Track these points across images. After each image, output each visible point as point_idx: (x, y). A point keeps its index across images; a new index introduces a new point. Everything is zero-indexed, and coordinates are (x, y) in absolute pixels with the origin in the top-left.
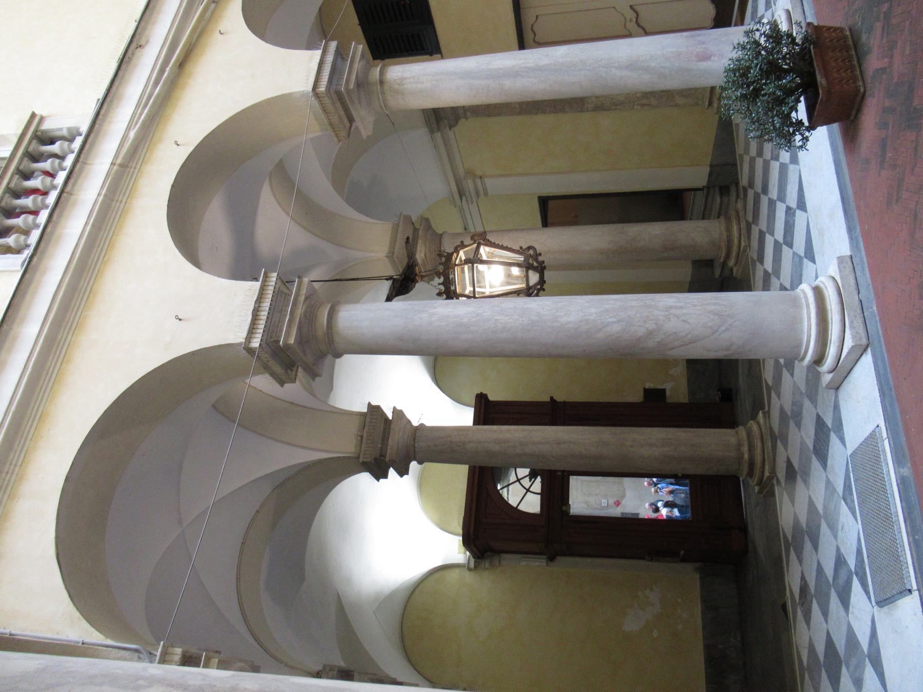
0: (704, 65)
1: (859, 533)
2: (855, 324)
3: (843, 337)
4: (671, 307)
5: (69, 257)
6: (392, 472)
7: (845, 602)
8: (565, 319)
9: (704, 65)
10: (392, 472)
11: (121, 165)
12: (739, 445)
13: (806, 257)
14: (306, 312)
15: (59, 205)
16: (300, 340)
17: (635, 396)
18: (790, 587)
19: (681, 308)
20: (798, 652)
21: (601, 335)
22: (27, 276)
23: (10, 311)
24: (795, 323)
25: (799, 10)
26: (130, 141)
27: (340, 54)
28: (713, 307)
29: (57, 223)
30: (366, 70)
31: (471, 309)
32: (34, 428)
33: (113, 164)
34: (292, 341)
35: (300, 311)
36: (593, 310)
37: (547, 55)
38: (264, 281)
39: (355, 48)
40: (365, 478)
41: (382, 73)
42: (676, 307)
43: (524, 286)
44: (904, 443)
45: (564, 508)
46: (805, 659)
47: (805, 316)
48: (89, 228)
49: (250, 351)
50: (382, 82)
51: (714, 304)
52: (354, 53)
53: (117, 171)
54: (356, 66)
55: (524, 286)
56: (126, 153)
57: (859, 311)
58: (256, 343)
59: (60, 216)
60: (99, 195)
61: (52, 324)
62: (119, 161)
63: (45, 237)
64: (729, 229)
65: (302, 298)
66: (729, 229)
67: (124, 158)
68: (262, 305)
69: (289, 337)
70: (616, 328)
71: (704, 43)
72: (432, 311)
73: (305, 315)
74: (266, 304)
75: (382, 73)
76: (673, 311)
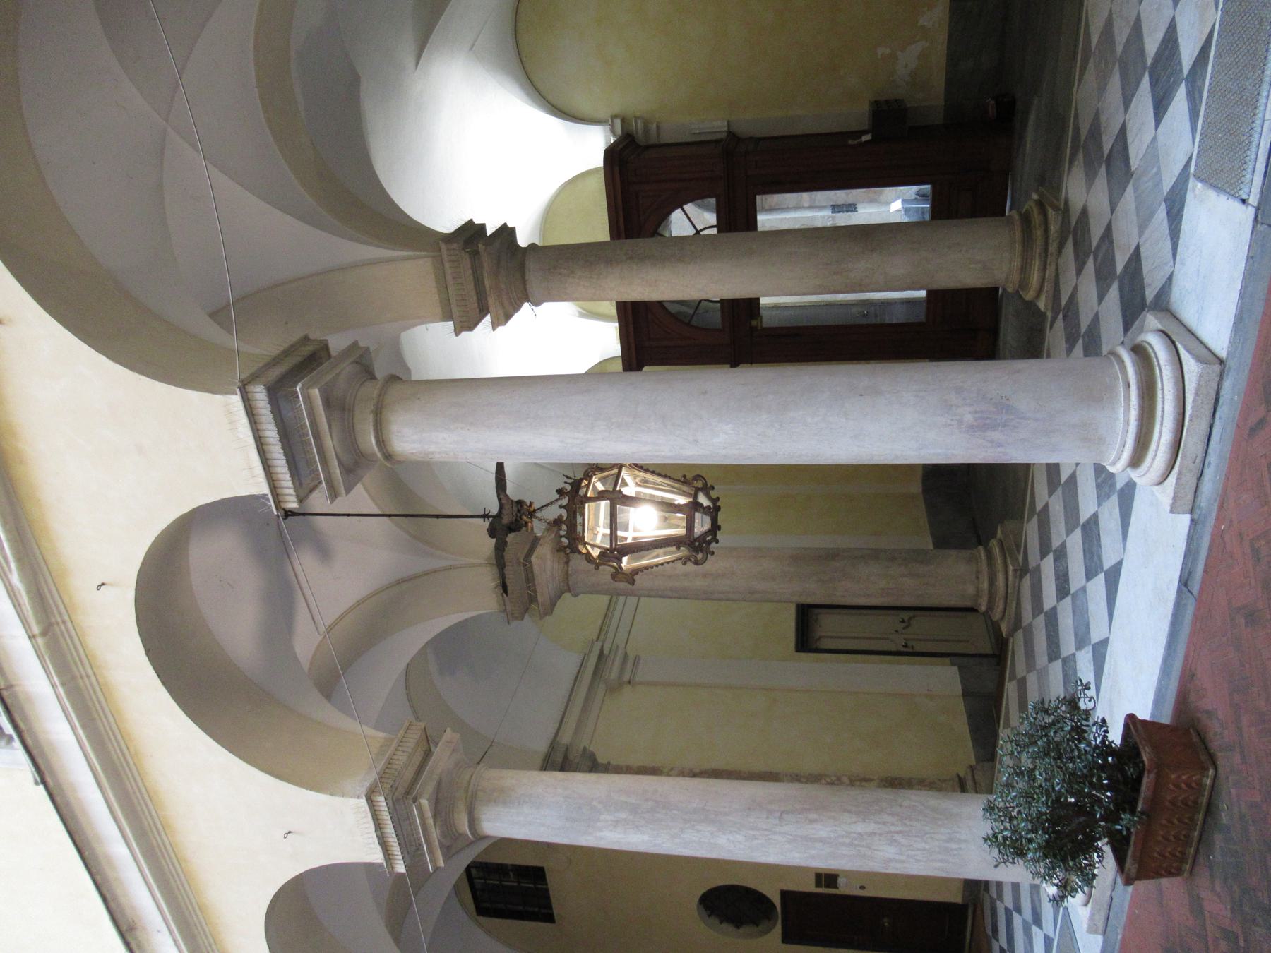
1: (1211, 33)
2: (1097, 917)
4: (890, 860)
5: (90, 773)
7: (1161, 106)
11: (44, 633)
12: (978, 595)
13: (1106, 574)
15: (12, 709)
17: (850, 113)
18: (1076, 110)
19: (903, 862)
20: (1087, 25)
22: (58, 799)
23: (77, 838)
25: (1204, 426)
26: (24, 593)
28: (940, 864)
29: (30, 729)
32: (79, 647)
33: (31, 637)
35: (435, 834)
37: (696, 441)
39: (308, 399)
42: (896, 861)
43: (681, 531)
45: (754, 323)
46: (1095, 39)
48: (80, 731)
51: (941, 861)
52: (314, 424)
53: (48, 646)
54: (329, 443)
55: (681, 531)
56: (34, 608)
57: (1106, 907)
59: (26, 719)
60: (54, 686)
61: (108, 778)
62: (36, 630)
63: (35, 752)
64: (1024, 269)
65: (430, 821)
66: (1024, 269)
67: (39, 622)
71: (1000, 445)
72: (598, 834)
73: (444, 835)
74: (390, 830)
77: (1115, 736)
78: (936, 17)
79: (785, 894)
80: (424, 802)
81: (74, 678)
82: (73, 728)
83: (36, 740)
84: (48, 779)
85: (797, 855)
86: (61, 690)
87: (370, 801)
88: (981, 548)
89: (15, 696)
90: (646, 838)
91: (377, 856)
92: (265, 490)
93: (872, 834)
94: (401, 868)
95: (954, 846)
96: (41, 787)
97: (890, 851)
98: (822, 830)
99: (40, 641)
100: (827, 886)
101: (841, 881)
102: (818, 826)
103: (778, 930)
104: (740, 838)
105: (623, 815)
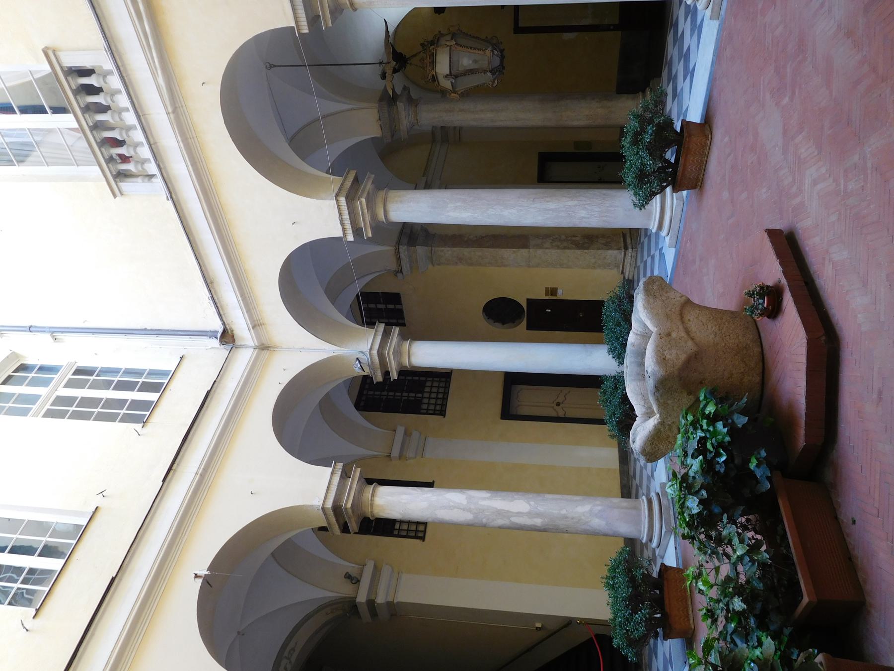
4: (583, 218)
11: (174, 112)
29: (165, 167)
31: (469, 214)
33: (168, 114)
35: (368, 218)
36: (540, 218)
62: (170, 110)
65: (366, 211)
77: (678, 127)
78: (658, 663)
79: (530, 301)
80: (363, 200)
81: (187, 139)
82: (187, 166)
83: (168, 175)
84: (173, 196)
85: (540, 218)
86: (181, 144)
87: (337, 200)
88: (616, 21)
89: (157, 147)
90: (469, 214)
91: (339, 234)
92: (293, 24)
93: (576, 205)
94: (350, 238)
95: (612, 209)
96: (170, 202)
97: (583, 213)
98: (552, 205)
99: (172, 116)
100: (552, 295)
101: (560, 291)
102: (550, 203)
103: (525, 322)
104: (514, 211)
105: (459, 204)
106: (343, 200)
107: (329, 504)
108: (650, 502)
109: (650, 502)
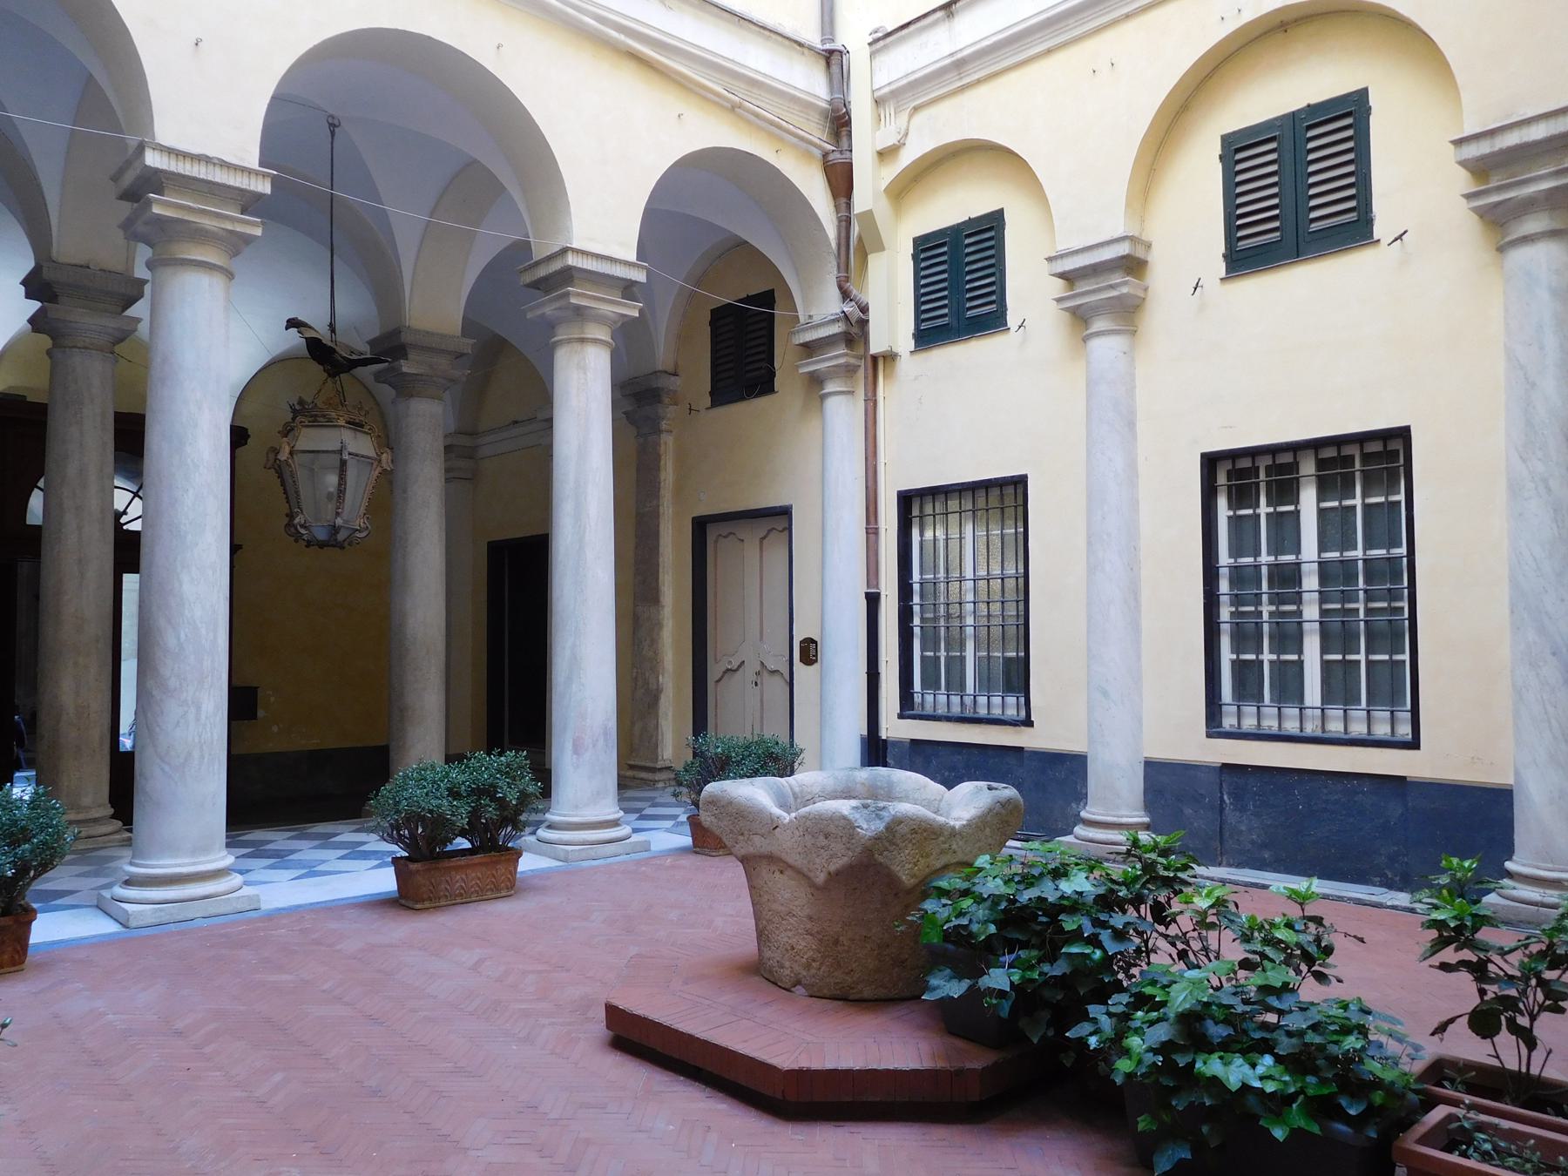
0: (569, 746)
3: (141, 905)
4: (199, 709)
6: (35, 305)
8: (185, 578)
9: (569, 746)
10: (35, 305)
14: (207, 231)
16: (161, 221)
19: (198, 720)
21: (162, 622)
24: (172, 849)
27: (628, 289)
30: (600, 319)
34: (156, 210)
38: (257, 173)
40: (28, 265)
41: (595, 341)
44: (916, 599)
47: (179, 861)
49: (141, 148)
50: (582, 340)
58: (152, 159)
68: (218, 169)
69: (161, 206)
70: (171, 641)
75: (595, 341)
76: (193, 710)
106: (836, 329)
107: (572, 260)
108: (615, 823)
109: (615, 823)
